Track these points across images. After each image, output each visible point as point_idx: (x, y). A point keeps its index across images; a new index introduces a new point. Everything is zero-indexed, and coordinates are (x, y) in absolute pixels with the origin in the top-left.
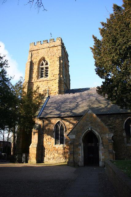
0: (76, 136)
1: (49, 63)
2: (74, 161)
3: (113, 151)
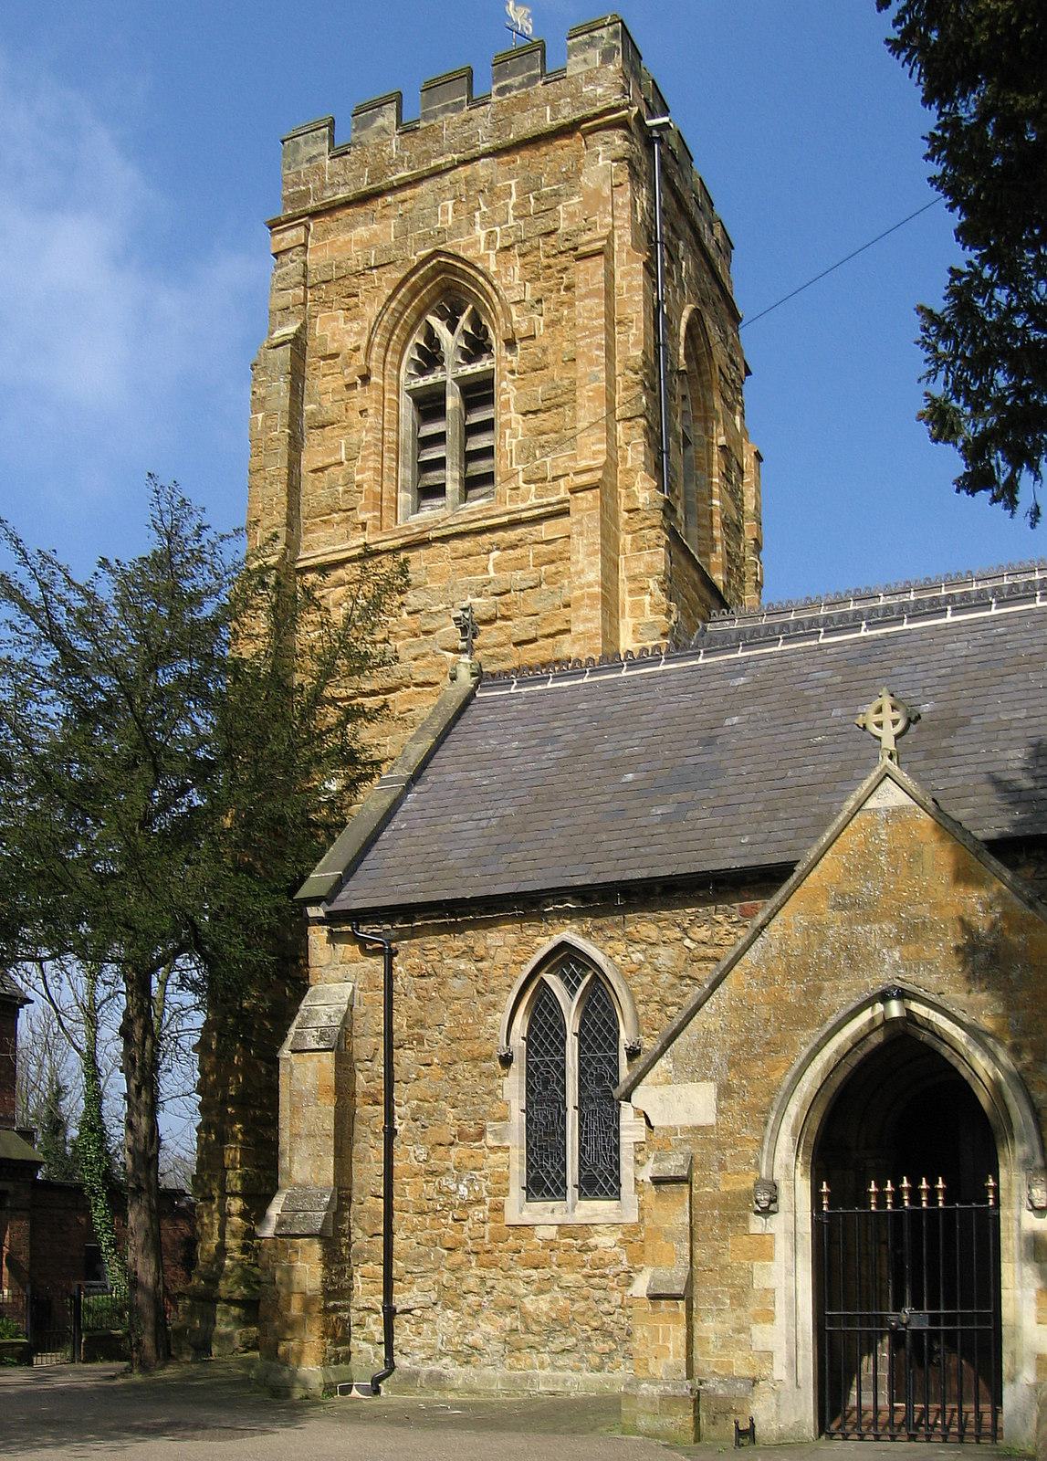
0: (725, 1092)
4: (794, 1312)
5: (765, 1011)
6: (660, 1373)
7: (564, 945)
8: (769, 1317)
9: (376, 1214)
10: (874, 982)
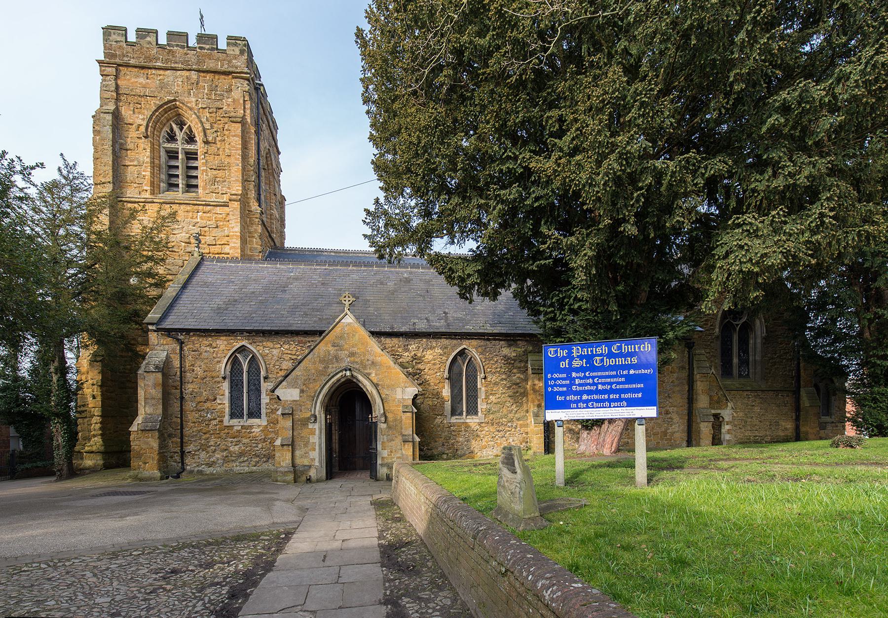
0: (302, 391)
1: (199, 138)
2: (294, 465)
3: (415, 435)
4: (320, 448)
5: (313, 371)
6: (284, 465)
7: (243, 346)
8: (314, 450)
9: (178, 423)
10: (343, 365)
